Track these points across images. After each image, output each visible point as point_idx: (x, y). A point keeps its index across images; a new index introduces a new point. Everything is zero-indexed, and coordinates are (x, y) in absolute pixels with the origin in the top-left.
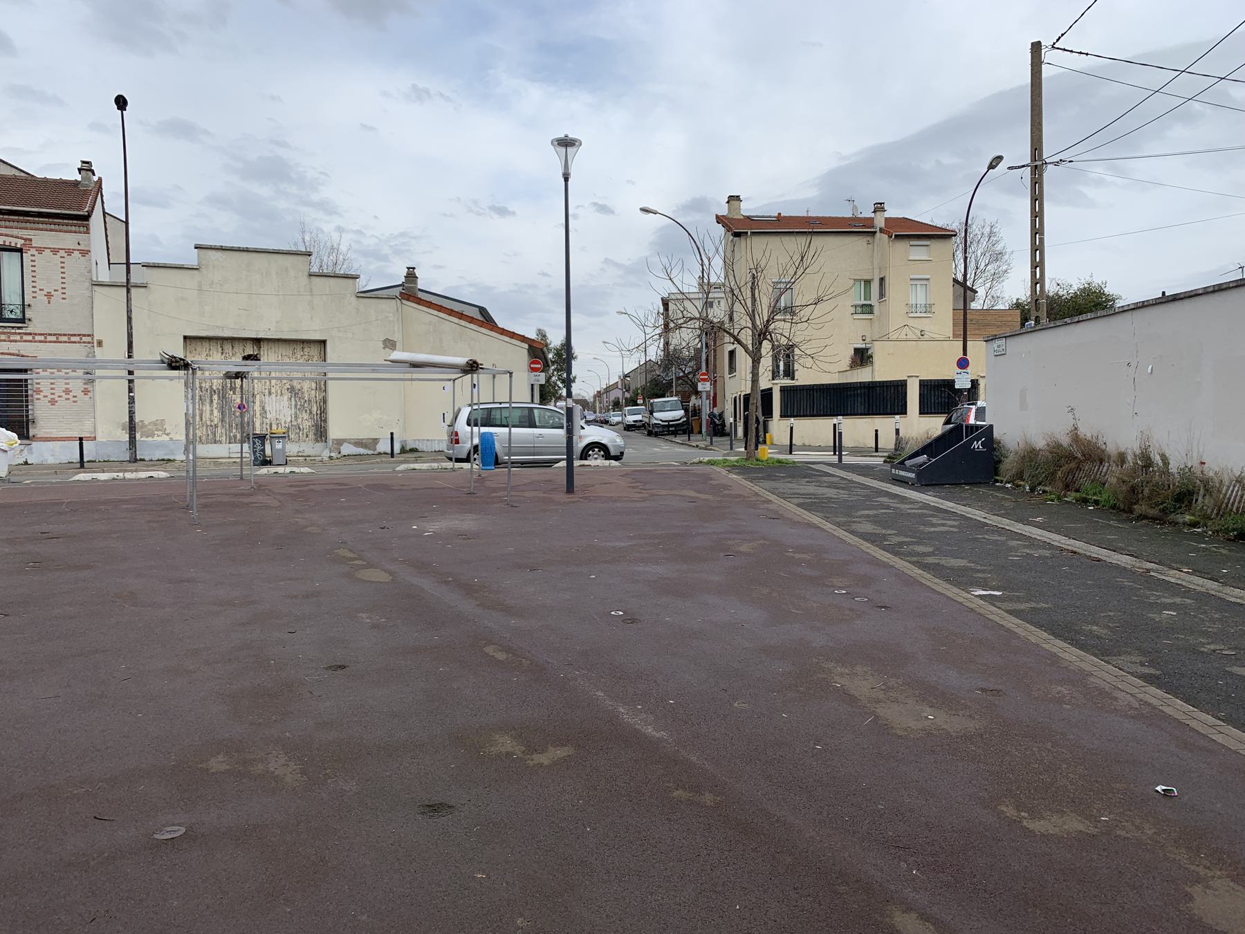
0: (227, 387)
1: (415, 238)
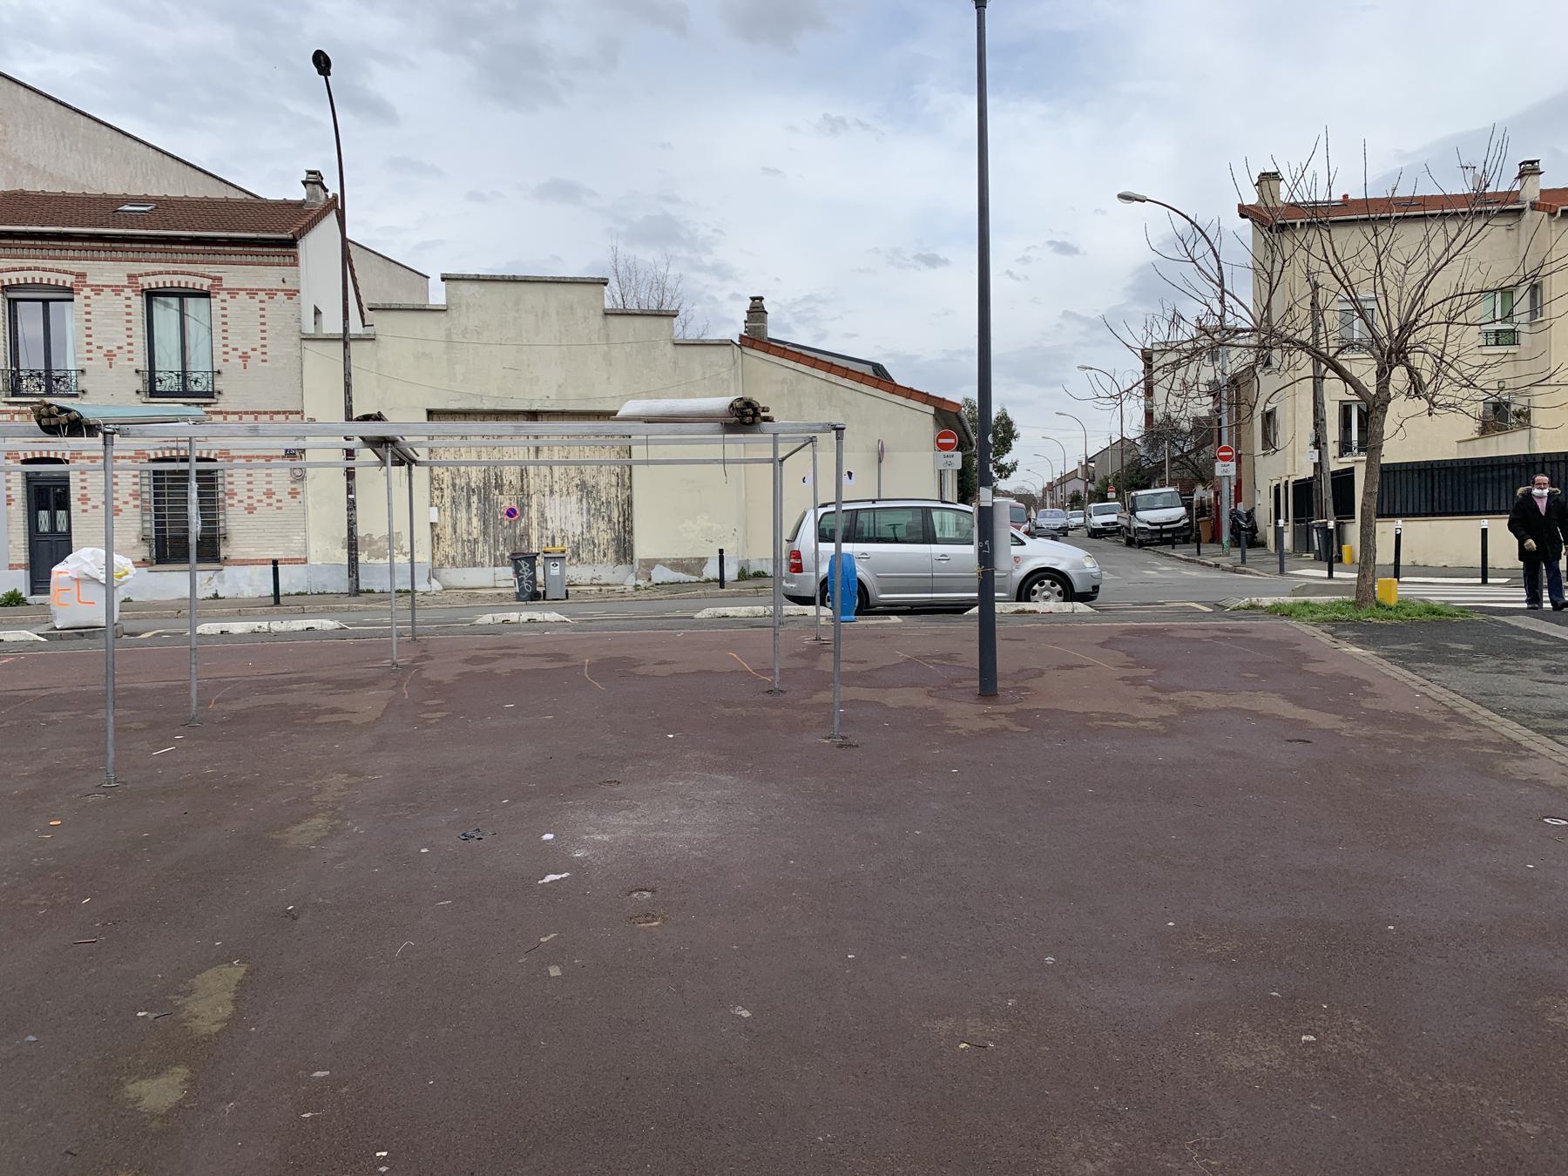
0: (491, 483)
1: (821, 302)
